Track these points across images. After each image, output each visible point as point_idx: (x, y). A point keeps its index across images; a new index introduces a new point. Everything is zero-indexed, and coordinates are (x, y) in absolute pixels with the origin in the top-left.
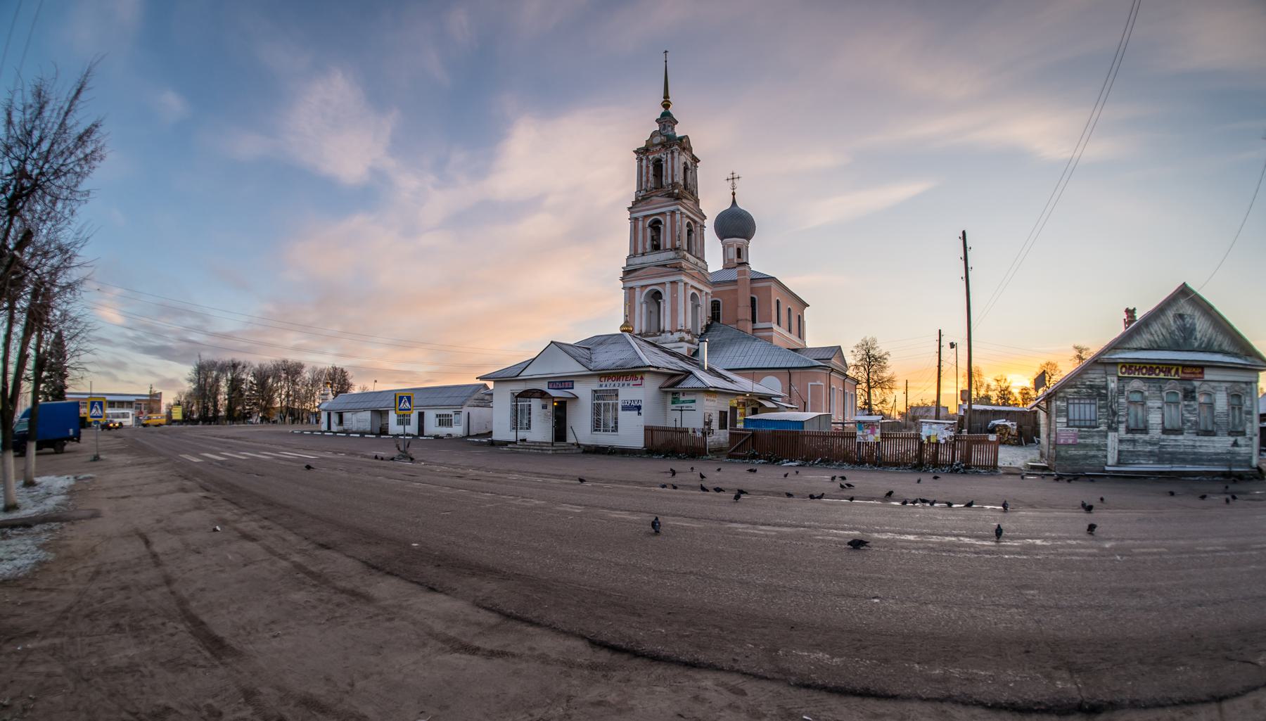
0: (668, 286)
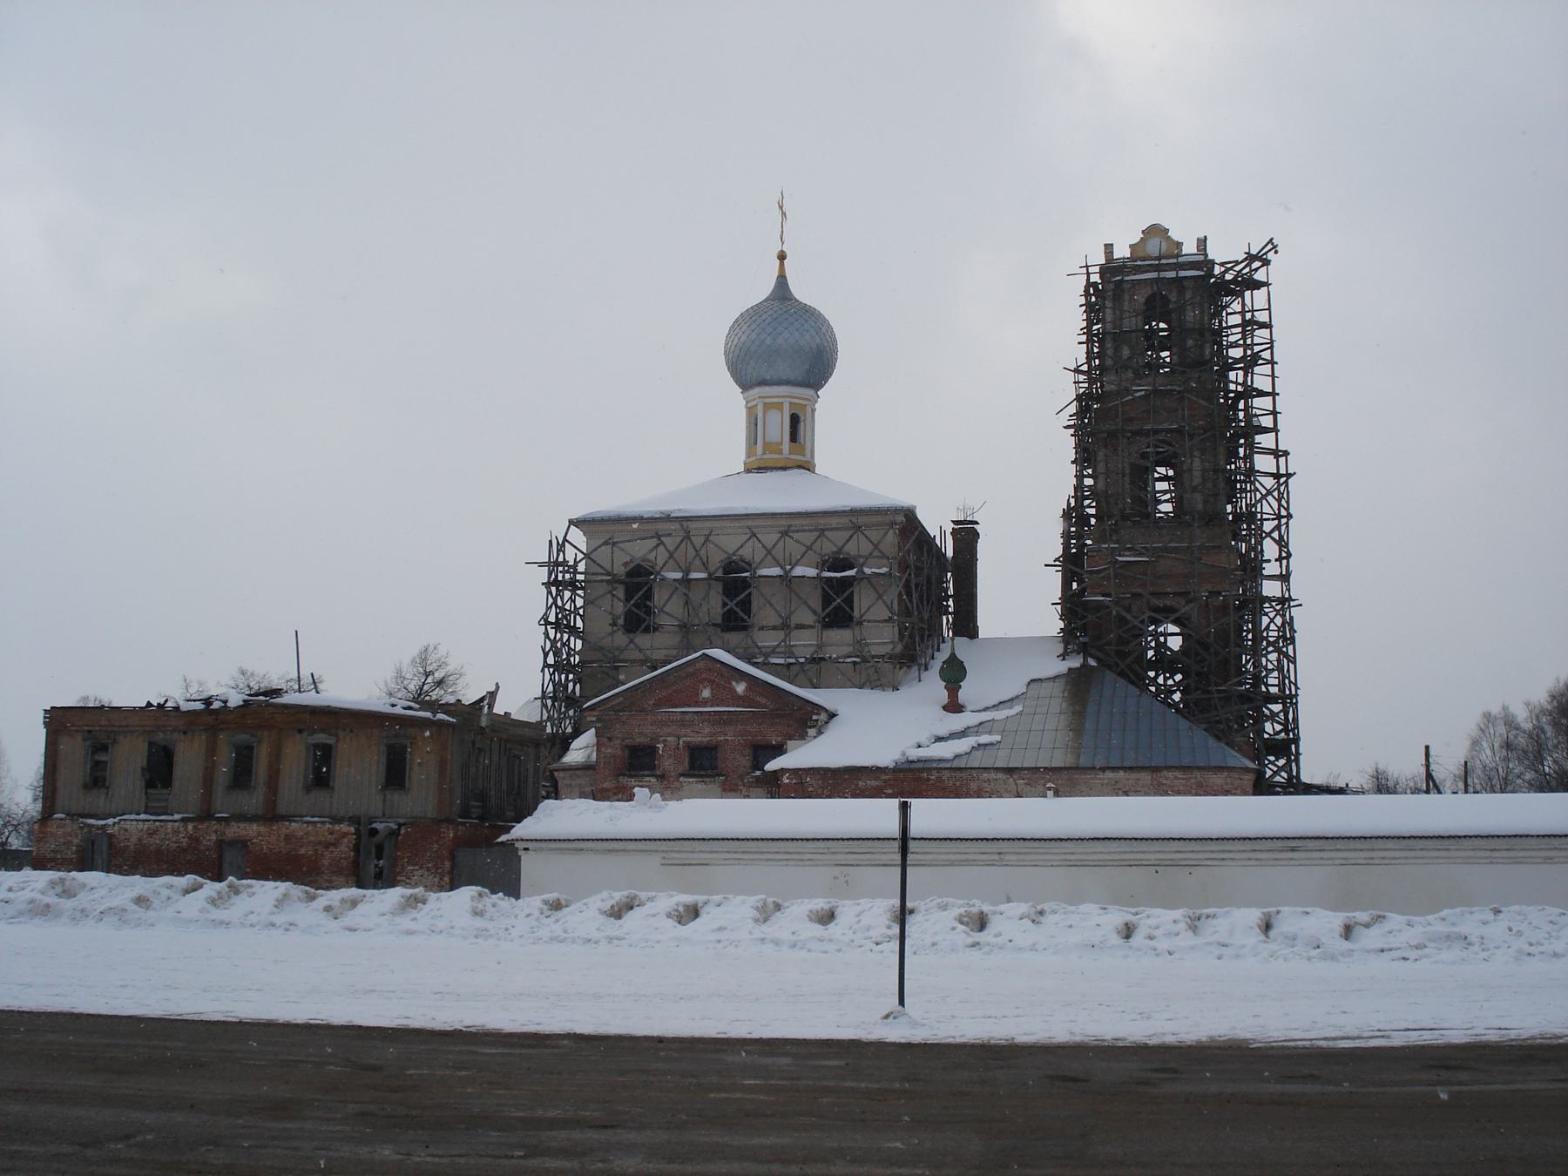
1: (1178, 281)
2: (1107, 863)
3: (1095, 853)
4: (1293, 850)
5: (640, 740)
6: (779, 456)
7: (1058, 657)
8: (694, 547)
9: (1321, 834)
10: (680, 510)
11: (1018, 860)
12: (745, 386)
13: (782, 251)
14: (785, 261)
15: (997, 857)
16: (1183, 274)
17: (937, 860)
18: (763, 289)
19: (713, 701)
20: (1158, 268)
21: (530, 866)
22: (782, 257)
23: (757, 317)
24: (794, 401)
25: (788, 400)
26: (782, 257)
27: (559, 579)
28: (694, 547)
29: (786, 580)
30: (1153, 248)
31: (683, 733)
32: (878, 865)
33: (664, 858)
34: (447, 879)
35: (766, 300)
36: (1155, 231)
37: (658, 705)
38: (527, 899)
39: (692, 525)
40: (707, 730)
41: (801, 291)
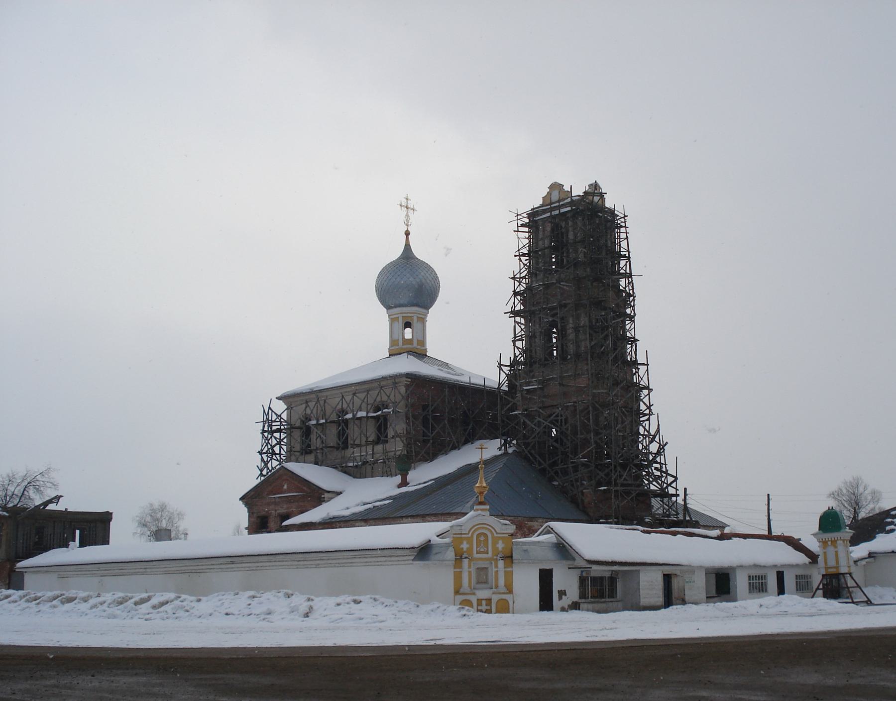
1: (561, 214)
2: (175, 572)
3: (202, 565)
4: (233, 563)
5: (263, 513)
6: (397, 347)
7: (58, 490)
8: (346, 402)
9: (229, 555)
10: (317, 387)
11: (151, 572)
12: (388, 308)
13: (407, 230)
14: (409, 236)
15: (144, 570)
16: (563, 210)
17: (129, 573)
18: (396, 252)
19: (288, 491)
20: (559, 207)
21: (28, 579)
22: (407, 234)
23: (398, 266)
24: (404, 315)
25: (401, 315)
26: (407, 234)
27: (269, 428)
28: (346, 402)
29: (318, 424)
30: (555, 196)
31: (277, 508)
32: (111, 576)
33: (59, 575)
34: (7, 586)
35: (399, 258)
36: (556, 187)
37: (268, 495)
38: (740, 602)
39: (320, 394)
40: (285, 506)
41: (419, 252)
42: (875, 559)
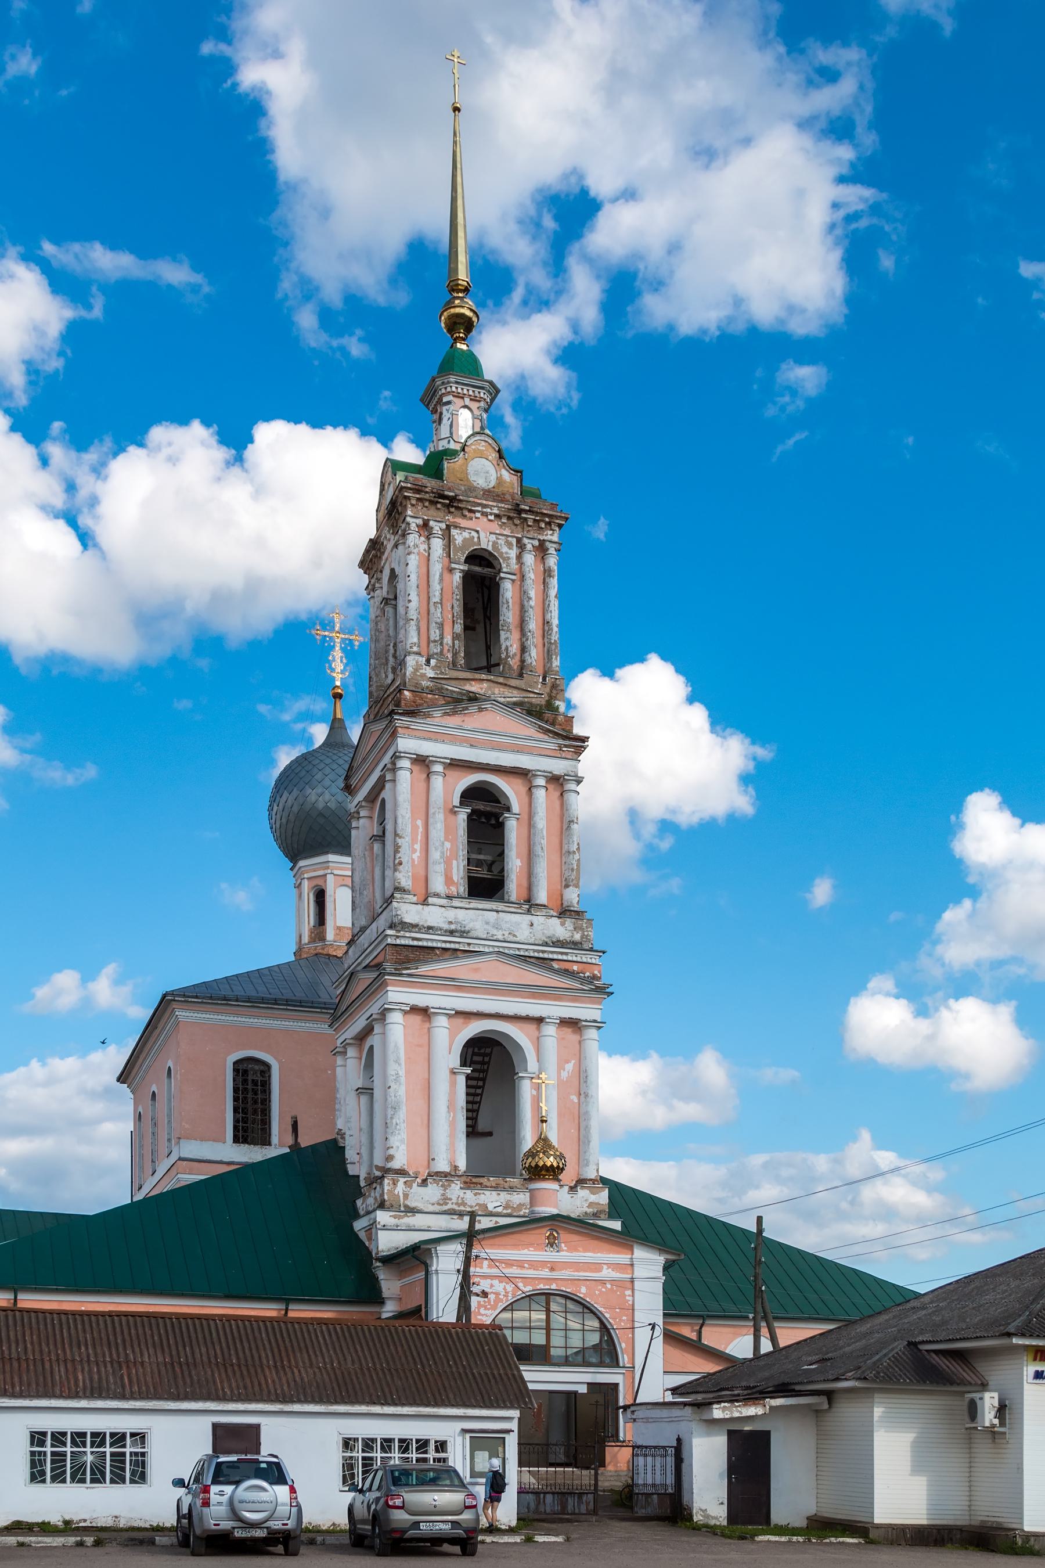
0: (550, 1030)
42: (830, 1402)
